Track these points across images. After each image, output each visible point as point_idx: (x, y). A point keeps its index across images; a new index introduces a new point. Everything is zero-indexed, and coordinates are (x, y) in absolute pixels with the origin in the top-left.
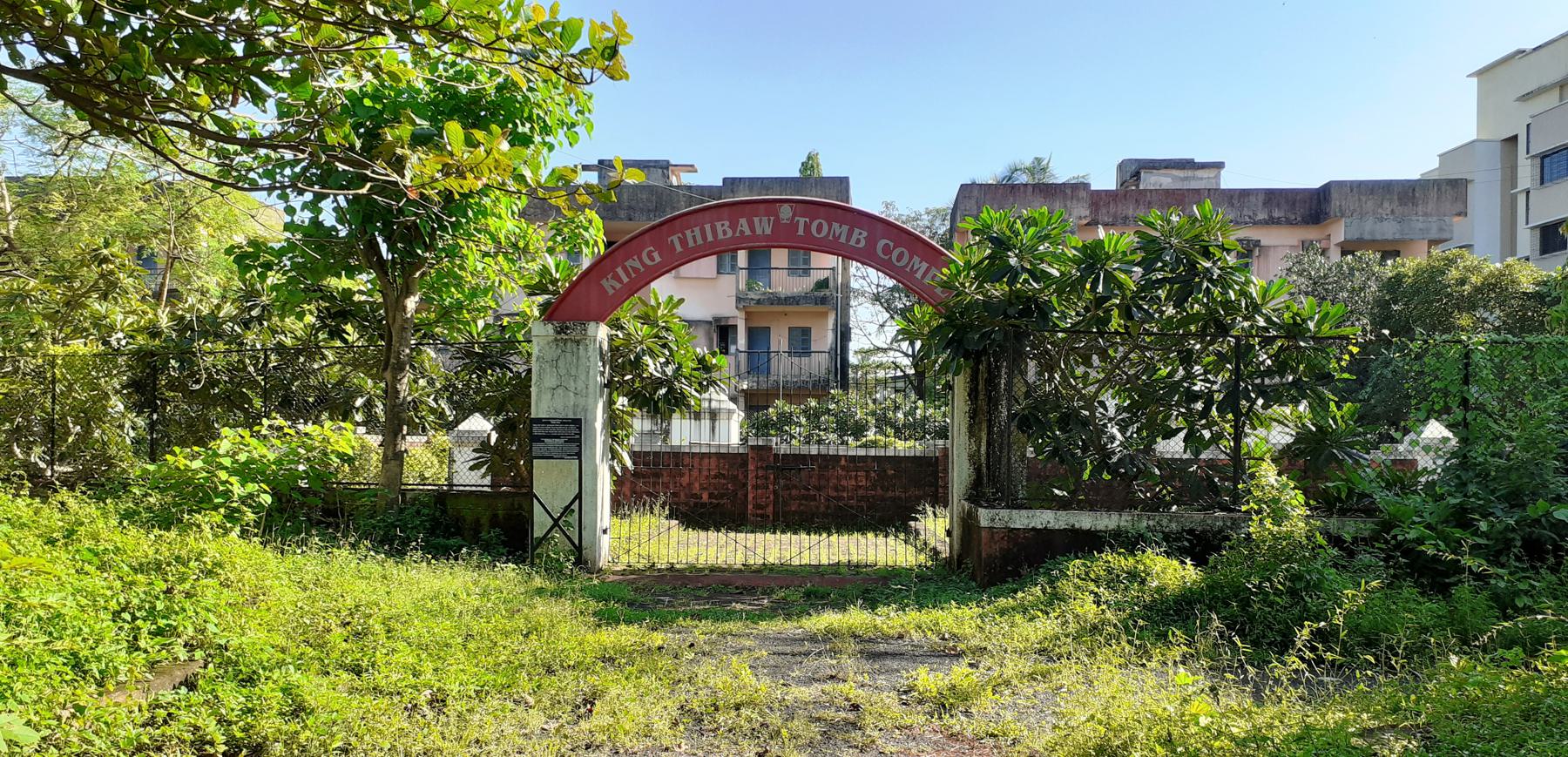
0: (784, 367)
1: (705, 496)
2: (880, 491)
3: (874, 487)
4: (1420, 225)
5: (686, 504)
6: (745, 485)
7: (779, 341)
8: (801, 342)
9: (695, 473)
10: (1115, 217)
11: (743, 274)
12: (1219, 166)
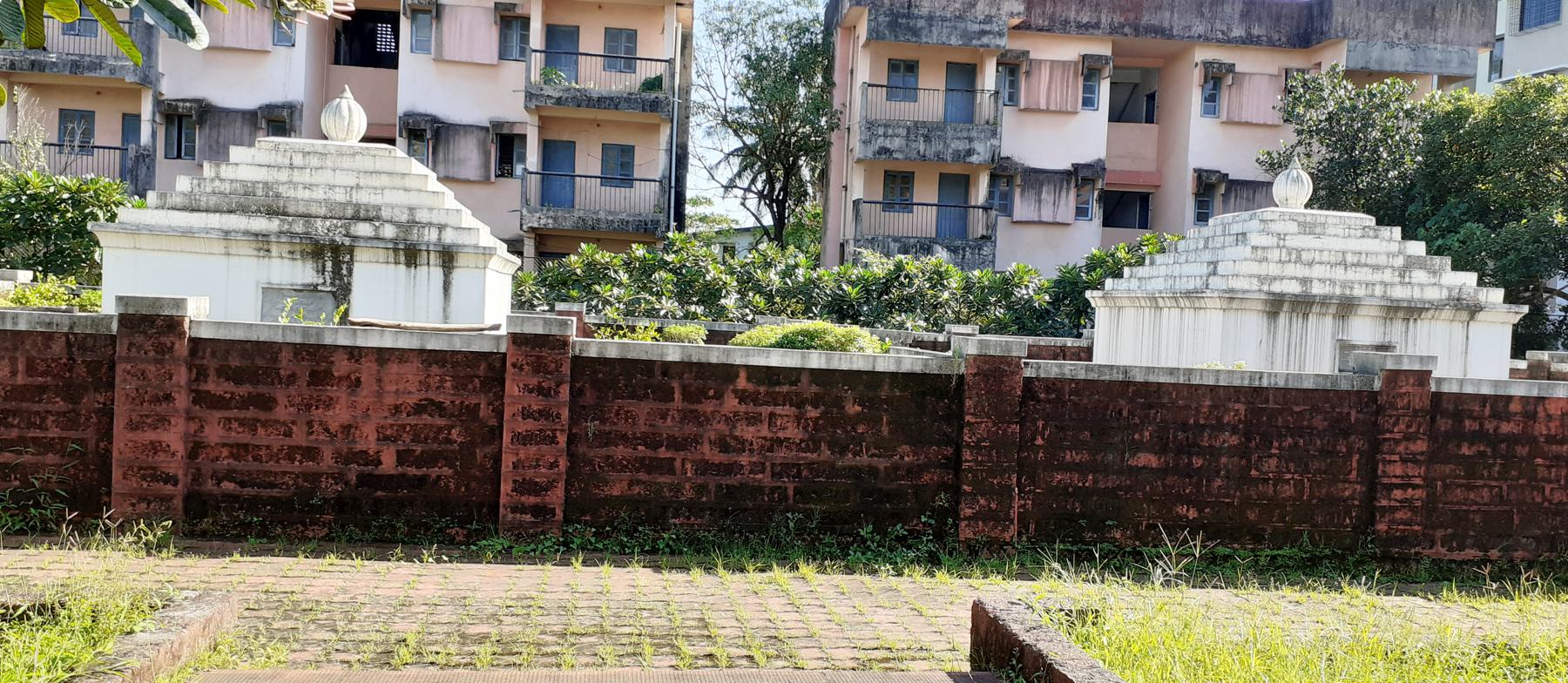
0: (594, 196)
1: (389, 463)
2: (826, 453)
3: (813, 444)
4: (1438, 56)
5: (339, 477)
6: (496, 433)
7: (588, 161)
8: (619, 168)
9: (365, 396)
10: (1052, 19)
11: (537, 60)
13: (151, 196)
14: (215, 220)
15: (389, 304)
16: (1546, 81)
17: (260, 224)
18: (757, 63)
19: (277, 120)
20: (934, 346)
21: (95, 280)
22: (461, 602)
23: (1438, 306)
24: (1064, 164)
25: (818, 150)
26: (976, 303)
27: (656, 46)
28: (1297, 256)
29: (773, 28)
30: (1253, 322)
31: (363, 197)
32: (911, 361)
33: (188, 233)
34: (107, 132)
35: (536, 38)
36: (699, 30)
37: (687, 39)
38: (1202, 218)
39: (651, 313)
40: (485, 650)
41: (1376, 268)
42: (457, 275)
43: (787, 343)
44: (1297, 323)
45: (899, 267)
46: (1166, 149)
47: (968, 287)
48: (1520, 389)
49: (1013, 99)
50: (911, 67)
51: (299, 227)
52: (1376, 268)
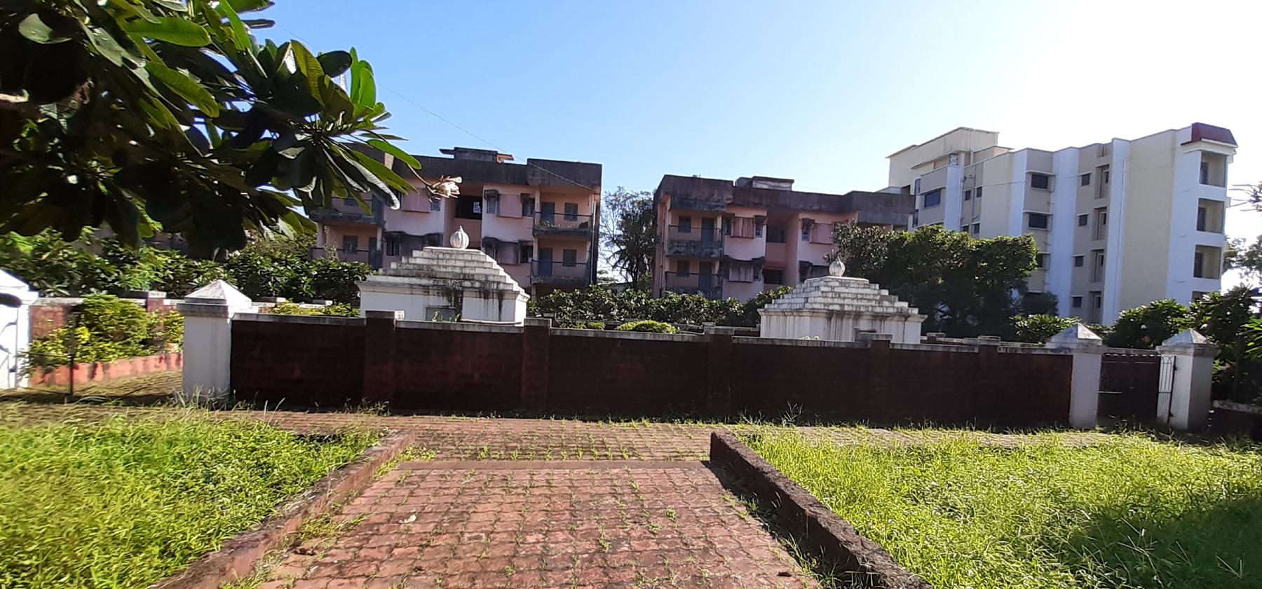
1: (477, 376)
7: (558, 256)
8: (570, 259)
11: (538, 216)
12: (792, 182)
13: (381, 271)
14: (406, 280)
15: (475, 313)
16: (935, 227)
17: (424, 282)
18: (626, 217)
19: (433, 240)
20: (698, 331)
21: (357, 304)
22: (504, 434)
23: (892, 315)
24: (749, 259)
25: (651, 252)
26: (714, 313)
27: (586, 210)
28: (839, 295)
29: (633, 203)
30: (822, 322)
31: (467, 271)
32: (688, 336)
33: (395, 285)
34: (363, 245)
35: (537, 208)
36: (603, 203)
37: (598, 207)
38: (802, 280)
39: (583, 318)
40: (515, 453)
41: (869, 300)
42: (504, 302)
43: (636, 329)
44: (839, 322)
45: (683, 298)
46: (790, 250)
47: (711, 307)
48: (924, 348)
49: (729, 232)
50: (688, 219)
51: (441, 283)
52: (869, 300)
